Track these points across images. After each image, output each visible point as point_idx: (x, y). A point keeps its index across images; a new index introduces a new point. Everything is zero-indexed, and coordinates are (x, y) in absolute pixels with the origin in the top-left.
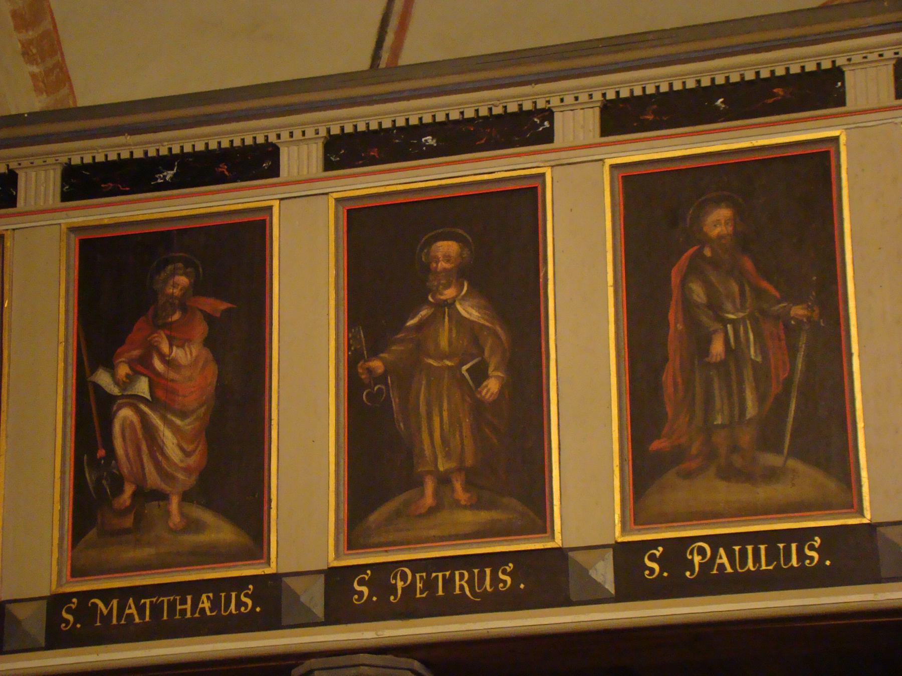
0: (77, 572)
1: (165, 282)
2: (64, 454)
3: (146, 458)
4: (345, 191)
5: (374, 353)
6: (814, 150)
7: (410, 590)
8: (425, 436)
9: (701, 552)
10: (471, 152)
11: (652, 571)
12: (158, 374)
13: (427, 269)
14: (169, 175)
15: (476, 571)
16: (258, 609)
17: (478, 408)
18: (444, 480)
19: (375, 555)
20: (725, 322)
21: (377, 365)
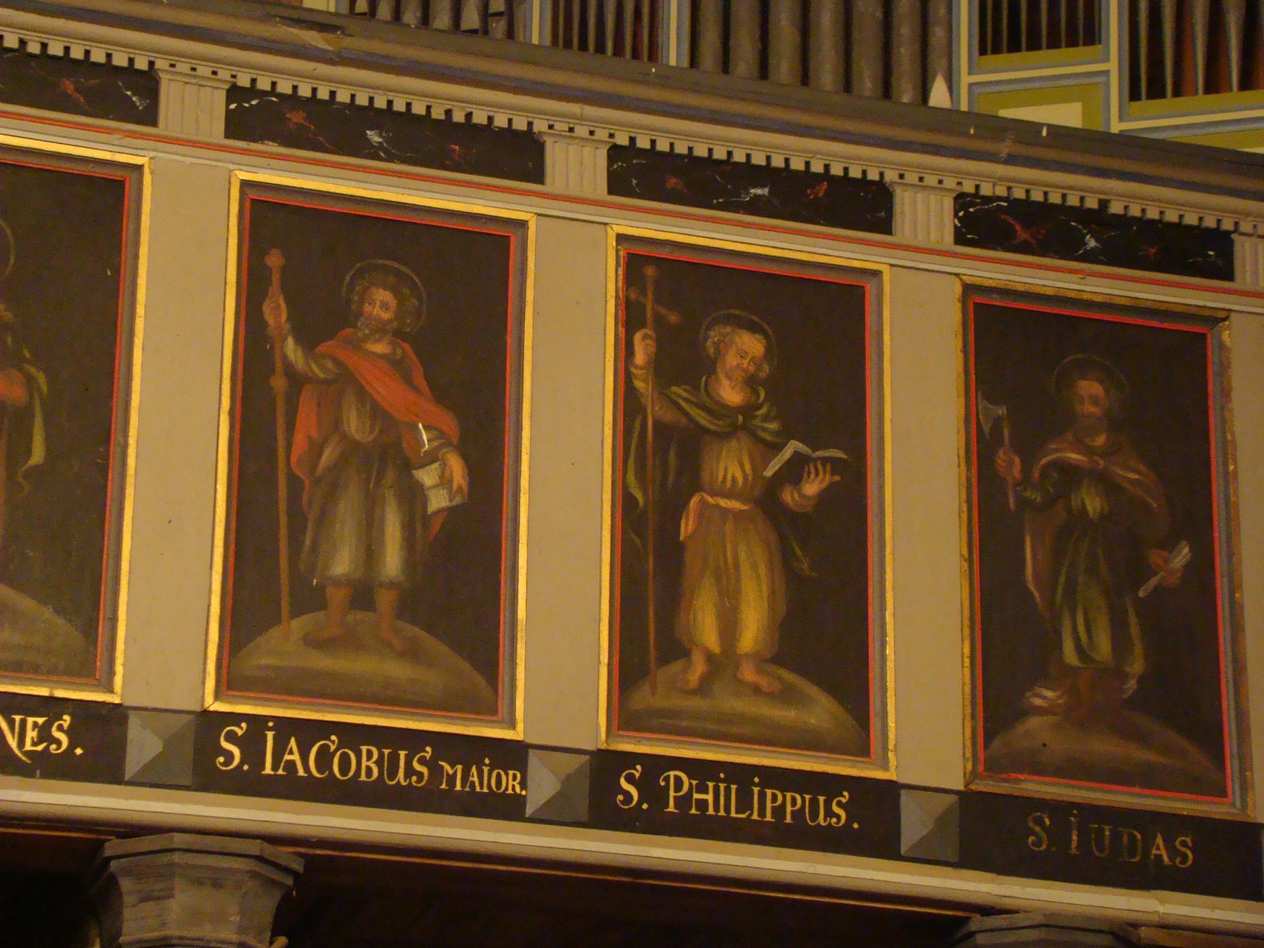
0: (993, 766)
4: (783, 249)
6: (262, 197)
10: (65, 111)
11: (628, 796)
15: (386, 752)
16: (246, 767)
19: (450, 721)
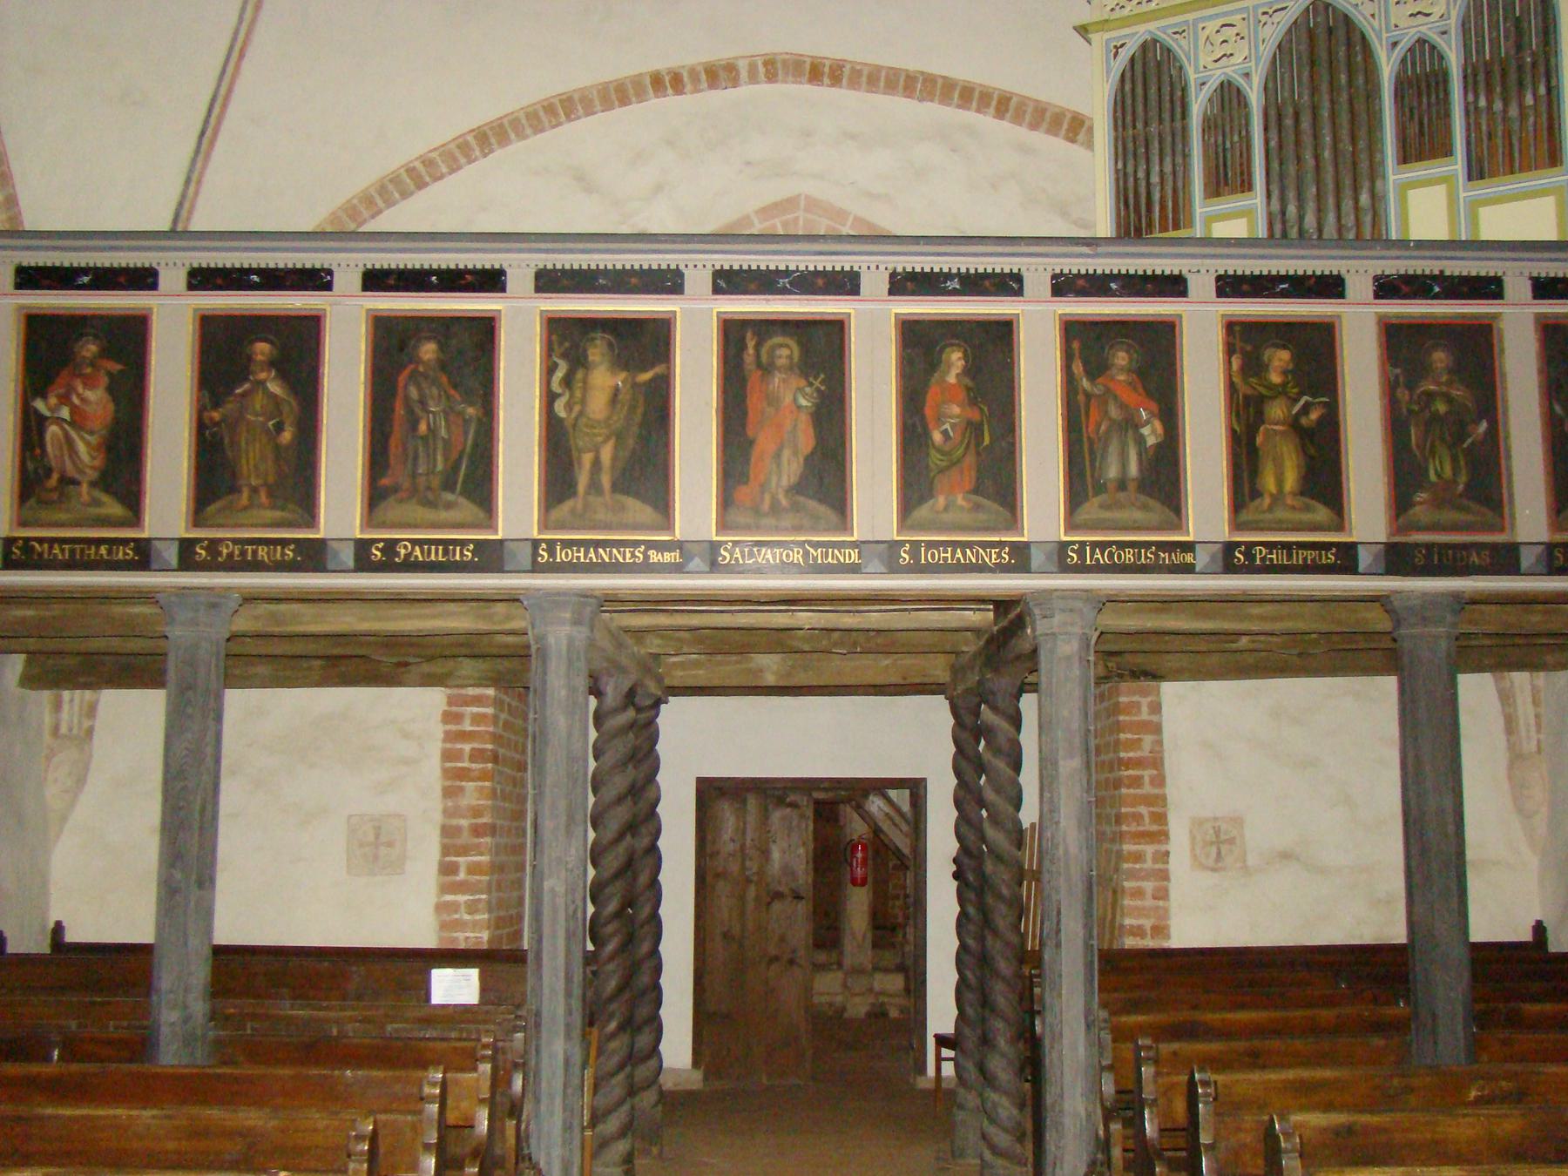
0: (1399, 530)
1: (82, 347)
2: (1140, 443)
3: (66, 458)
5: (216, 405)
7: (230, 555)
8: (244, 461)
9: (406, 547)
12: (76, 406)
13: (250, 359)
14: (86, 279)
17: (277, 448)
18: (255, 490)
20: (429, 412)
21: (216, 415)
